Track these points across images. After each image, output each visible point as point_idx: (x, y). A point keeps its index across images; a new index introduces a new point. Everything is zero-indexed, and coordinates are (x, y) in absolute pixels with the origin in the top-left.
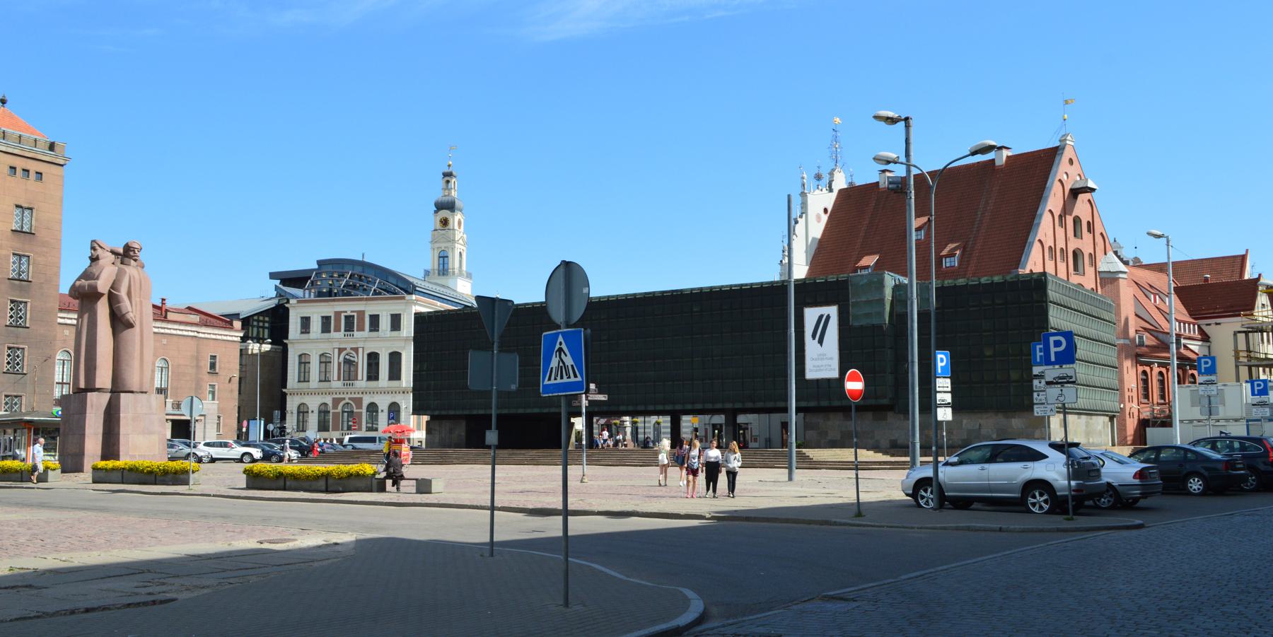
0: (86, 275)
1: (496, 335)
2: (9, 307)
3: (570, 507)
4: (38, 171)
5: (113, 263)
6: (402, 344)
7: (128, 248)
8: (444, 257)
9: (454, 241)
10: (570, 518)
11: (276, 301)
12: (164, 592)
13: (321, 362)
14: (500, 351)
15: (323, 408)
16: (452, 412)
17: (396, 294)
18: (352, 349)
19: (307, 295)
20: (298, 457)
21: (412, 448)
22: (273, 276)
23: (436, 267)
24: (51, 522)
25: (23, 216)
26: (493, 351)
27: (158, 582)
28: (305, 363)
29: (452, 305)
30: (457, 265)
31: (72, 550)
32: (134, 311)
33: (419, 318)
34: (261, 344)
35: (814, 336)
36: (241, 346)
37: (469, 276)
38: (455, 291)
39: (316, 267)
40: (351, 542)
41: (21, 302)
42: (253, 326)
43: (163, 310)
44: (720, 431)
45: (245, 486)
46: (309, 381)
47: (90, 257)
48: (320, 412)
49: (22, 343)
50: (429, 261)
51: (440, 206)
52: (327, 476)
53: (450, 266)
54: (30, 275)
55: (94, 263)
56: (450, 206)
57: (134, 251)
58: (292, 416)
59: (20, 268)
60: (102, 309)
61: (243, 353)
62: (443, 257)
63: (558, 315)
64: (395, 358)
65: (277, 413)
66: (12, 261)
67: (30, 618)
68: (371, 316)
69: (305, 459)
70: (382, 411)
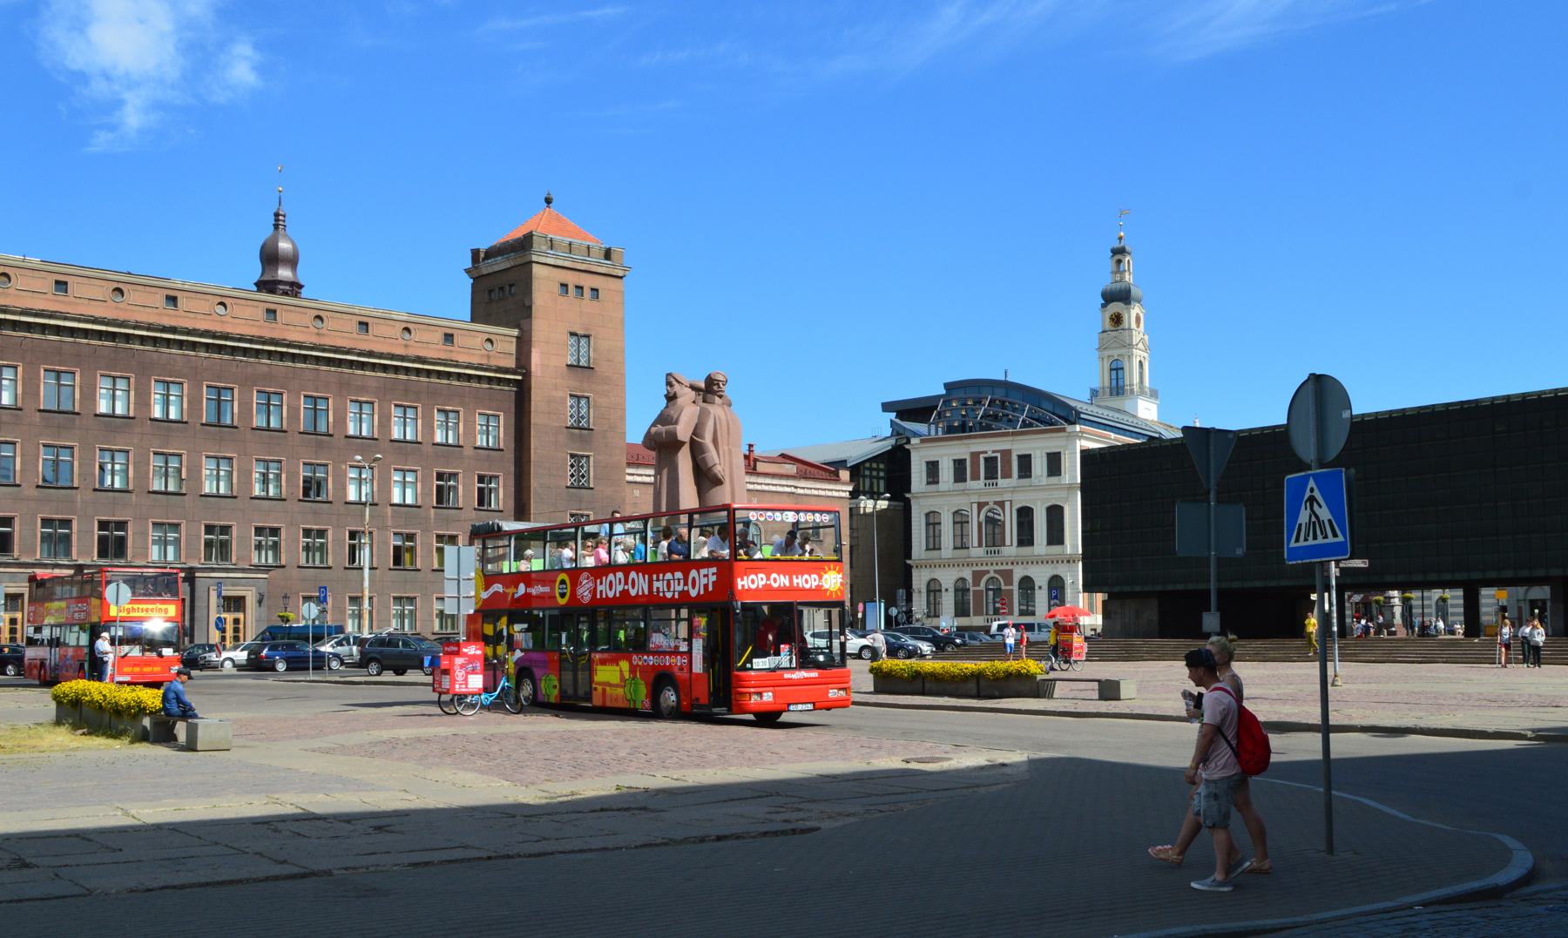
0: (663, 419)
1: (1213, 481)
2: (569, 464)
3: (1333, 721)
4: (594, 287)
5: (694, 402)
6: (1064, 494)
7: (710, 381)
8: (1117, 369)
9: (1130, 346)
10: (1332, 735)
11: (892, 441)
12: (803, 820)
13: (955, 523)
14: (1218, 501)
15: (960, 585)
16: (1138, 588)
17: (1052, 424)
18: (995, 503)
19: (933, 432)
20: (932, 651)
21: (1087, 639)
22: (887, 407)
23: (1107, 384)
24: (648, 733)
25: (579, 347)
26: (1209, 503)
27: (792, 808)
28: (934, 524)
29: (1132, 437)
30: (1136, 380)
31: (682, 767)
32: (722, 464)
33: (1087, 455)
34: (876, 500)
36: (850, 504)
37: (1154, 394)
38: (1135, 416)
39: (944, 392)
40: (1023, 762)
41: (582, 456)
42: (864, 476)
43: (752, 459)
44: (1543, 610)
45: (872, 689)
46: (940, 549)
47: (666, 396)
48: (956, 590)
49: (586, 510)
50: (1097, 376)
52: (978, 676)
53: (1127, 382)
54: (591, 420)
55: (672, 402)
57: (718, 384)
58: (920, 597)
59: (579, 412)
60: (684, 461)
61: (853, 512)
62: (1117, 370)
63: (1305, 447)
64: (1055, 514)
65: (901, 592)
66: (569, 404)
67: (657, 845)
68: (1020, 457)
69: (941, 654)
70: (1040, 588)
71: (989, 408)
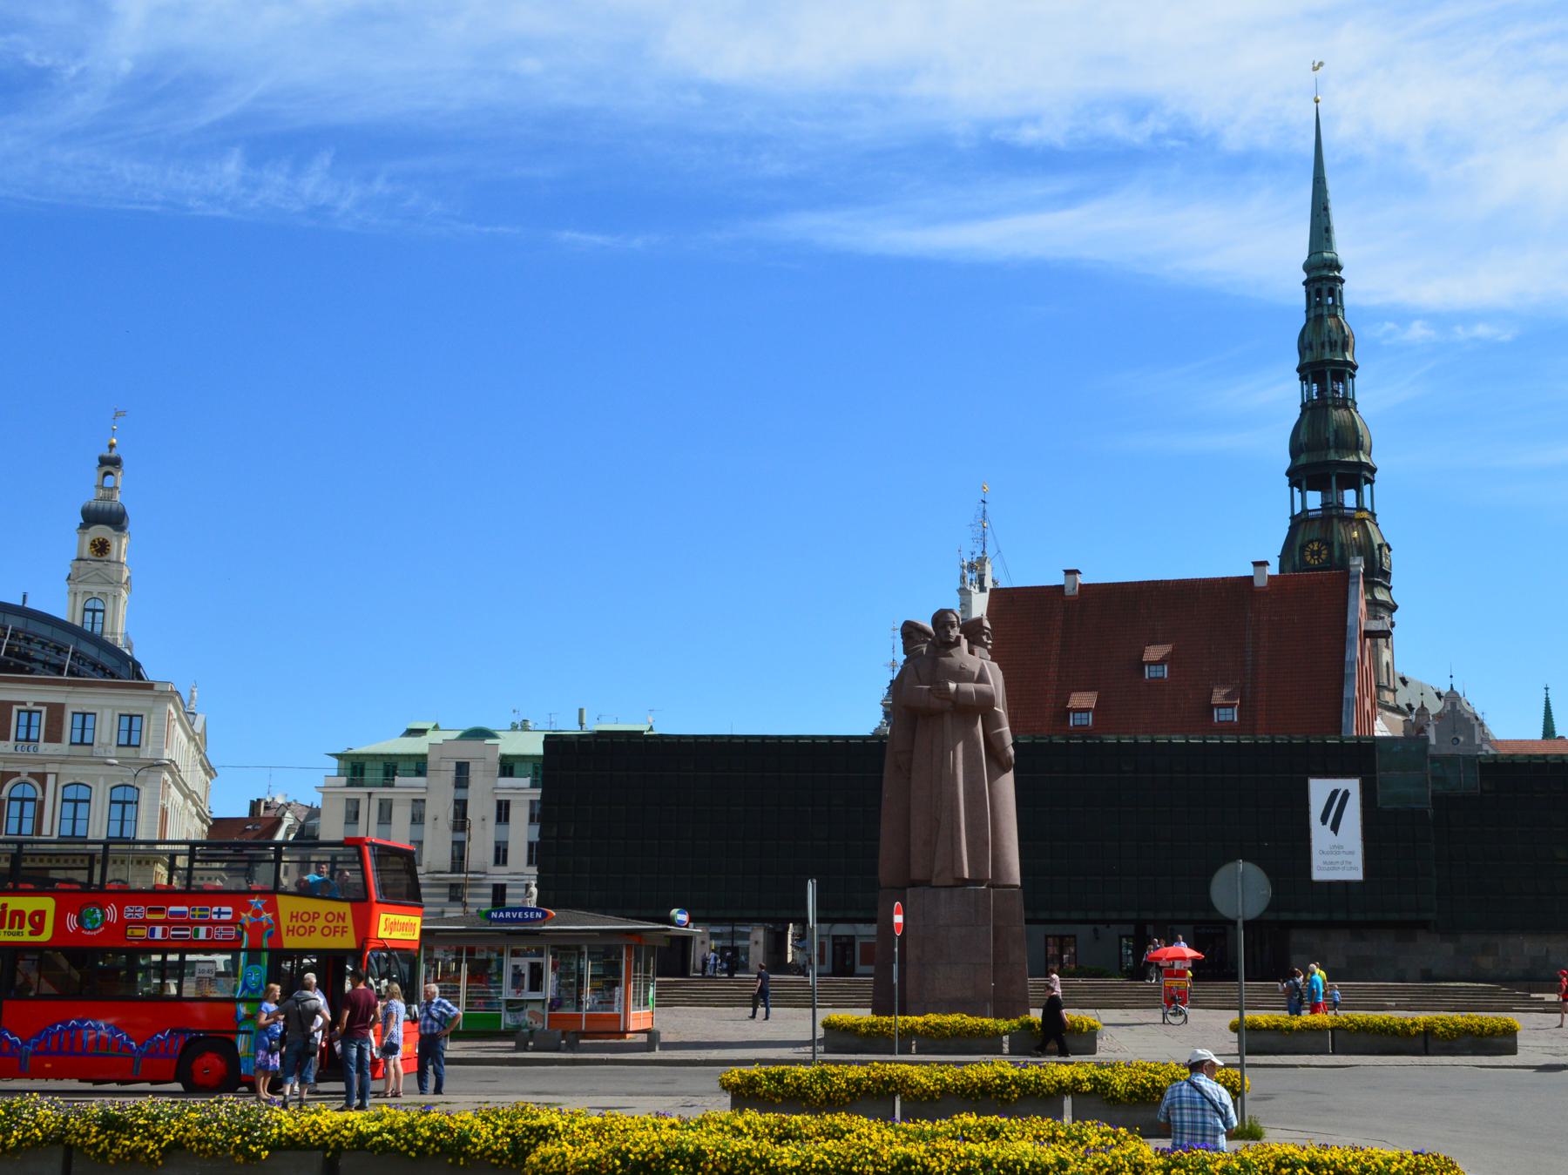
18: (30, 774)
35: (1324, 820)
51: (91, 517)
56: (116, 520)
71: (13, 642)
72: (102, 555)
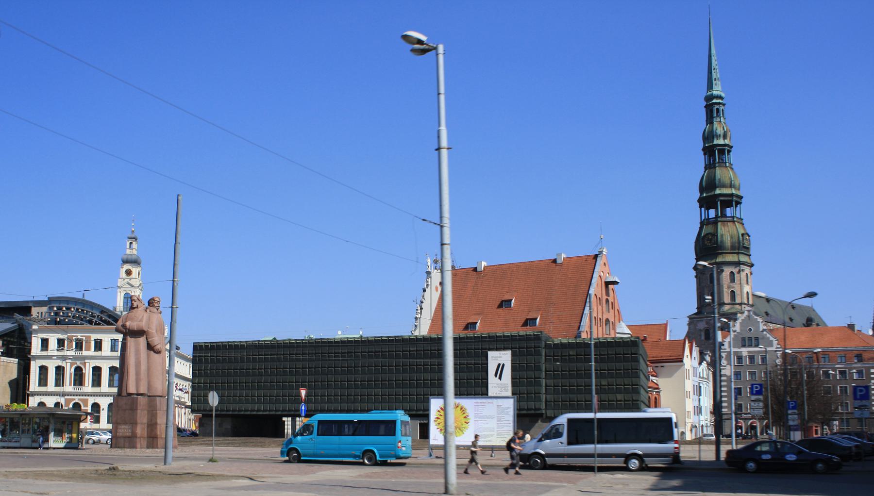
35: (496, 375)
72: (129, 276)
